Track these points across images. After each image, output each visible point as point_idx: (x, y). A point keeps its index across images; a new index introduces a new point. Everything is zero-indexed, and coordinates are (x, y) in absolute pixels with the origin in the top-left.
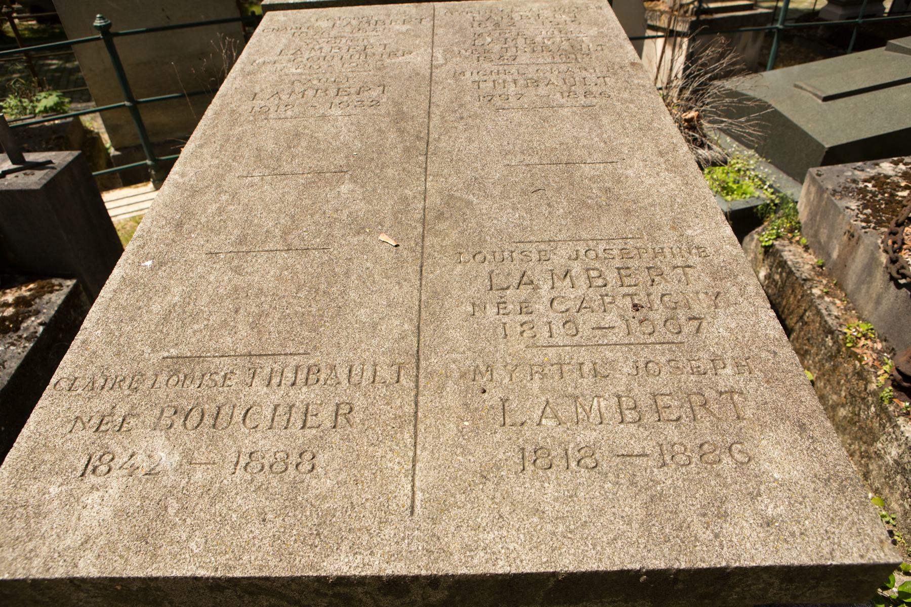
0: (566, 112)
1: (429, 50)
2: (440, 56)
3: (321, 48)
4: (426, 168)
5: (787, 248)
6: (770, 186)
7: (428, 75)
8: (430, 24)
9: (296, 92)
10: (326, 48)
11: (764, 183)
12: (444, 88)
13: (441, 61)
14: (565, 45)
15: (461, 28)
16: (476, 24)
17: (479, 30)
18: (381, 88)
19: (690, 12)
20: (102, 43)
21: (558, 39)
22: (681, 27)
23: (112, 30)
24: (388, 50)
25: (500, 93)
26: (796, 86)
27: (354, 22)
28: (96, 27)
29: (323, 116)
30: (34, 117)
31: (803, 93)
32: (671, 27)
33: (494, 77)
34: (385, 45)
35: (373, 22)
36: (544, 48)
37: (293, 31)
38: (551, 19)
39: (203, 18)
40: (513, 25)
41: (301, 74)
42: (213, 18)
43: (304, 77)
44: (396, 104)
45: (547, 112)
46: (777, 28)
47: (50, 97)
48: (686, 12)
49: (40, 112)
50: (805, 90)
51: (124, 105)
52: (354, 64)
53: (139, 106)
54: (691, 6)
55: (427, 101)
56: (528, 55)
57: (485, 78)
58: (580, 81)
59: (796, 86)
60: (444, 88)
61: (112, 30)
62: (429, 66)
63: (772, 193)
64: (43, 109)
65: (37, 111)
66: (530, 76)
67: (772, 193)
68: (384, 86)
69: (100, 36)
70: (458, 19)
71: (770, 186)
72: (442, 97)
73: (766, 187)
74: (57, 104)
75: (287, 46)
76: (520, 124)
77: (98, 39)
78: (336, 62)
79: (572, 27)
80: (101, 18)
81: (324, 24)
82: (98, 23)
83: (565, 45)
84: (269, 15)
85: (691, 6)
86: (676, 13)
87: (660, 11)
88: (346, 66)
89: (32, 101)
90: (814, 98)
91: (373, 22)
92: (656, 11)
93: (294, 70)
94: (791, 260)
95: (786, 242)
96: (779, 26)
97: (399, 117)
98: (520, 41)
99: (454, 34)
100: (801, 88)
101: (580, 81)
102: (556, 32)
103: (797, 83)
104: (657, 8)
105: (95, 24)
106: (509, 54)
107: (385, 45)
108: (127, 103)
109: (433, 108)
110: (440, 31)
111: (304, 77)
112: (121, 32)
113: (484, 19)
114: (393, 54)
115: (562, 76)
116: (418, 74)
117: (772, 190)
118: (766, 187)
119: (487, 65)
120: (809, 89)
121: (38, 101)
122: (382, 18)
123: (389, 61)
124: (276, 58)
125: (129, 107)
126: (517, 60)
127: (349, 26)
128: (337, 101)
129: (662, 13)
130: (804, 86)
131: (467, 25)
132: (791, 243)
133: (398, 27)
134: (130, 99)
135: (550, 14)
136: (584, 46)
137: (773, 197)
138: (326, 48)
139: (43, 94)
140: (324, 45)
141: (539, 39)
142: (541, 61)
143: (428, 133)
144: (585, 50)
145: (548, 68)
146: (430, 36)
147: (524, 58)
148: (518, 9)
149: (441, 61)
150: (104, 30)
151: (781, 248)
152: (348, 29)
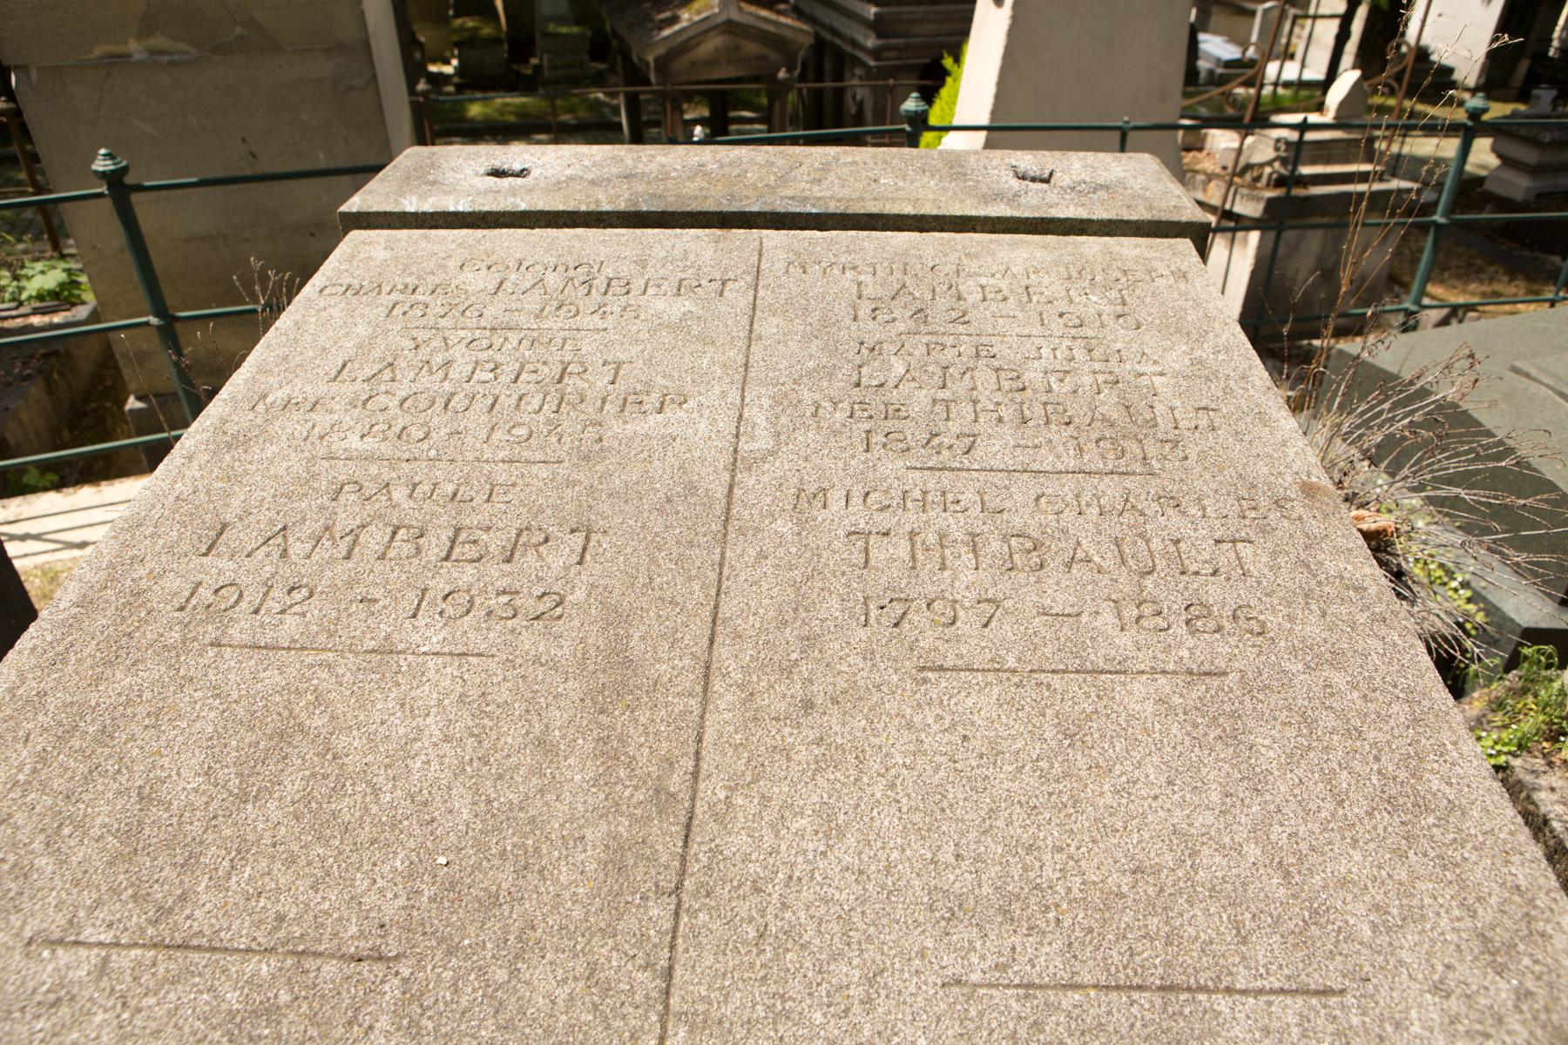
0: (1137, 696)
1: (734, 396)
2: (761, 421)
3: (448, 364)
4: (669, 973)
5: (1543, 781)
6: (1465, 585)
7: (720, 493)
8: (744, 302)
9: (337, 531)
10: (462, 360)
11: (1450, 574)
12: (762, 556)
13: (763, 442)
14: (1109, 403)
15: (825, 323)
16: (865, 310)
17: (873, 331)
18: (579, 539)
19: (1264, 180)
20: (107, 204)
21: (1087, 380)
22: (1250, 208)
23: (129, 180)
24: (622, 385)
25: (931, 590)
26: (1515, 370)
27: (553, 280)
28: (96, 172)
29: (387, 650)
30: (16, 308)
31: (1533, 387)
32: (1227, 207)
33: (912, 519)
34: (619, 365)
35: (600, 283)
36: (1059, 416)
37: (395, 296)
38: (1062, 306)
39: (322, 160)
40: (963, 319)
41: (370, 458)
42: (342, 163)
43: (374, 470)
44: (616, 618)
45: (1077, 695)
46: (1435, 223)
47: (52, 272)
48: (1257, 179)
49: (30, 298)
50: (1535, 380)
51: (147, 324)
52: (522, 432)
53: (178, 327)
54: (1268, 170)
55: (706, 613)
56: (1008, 434)
57: (885, 520)
58: (1165, 554)
59: (1515, 370)
60: (762, 556)
61: (129, 180)
62: (726, 458)
63: (1469, 600)
64: (34, 293)
65: (24, 296)
66: (1017, 522)
67: (1469, 600)
68: (589, 532)
69: (104, 189)
70: (818, 290)
71: (1465, 585)
72: (754, 598)
73: (1454, 584)
74: (62, 285)
75: (364, 348)
76: (995, 753)
77: (100, 195)
78: (476, 420)
79: (1119, 337)
80: (109, 156)
81: (478, 281)
82: (101, 165)
83: (1109, 403)
84: (355, 234)
85: (1268, 170)
86: (1236, 179)
87: (1205, 173)
88: (498, 435)
89: (16, 278)
90: (1558, 399)
91: (600, 283)
92: (1197, 172)
93: (354, 442)
94: (1559, 818)
95: (1539, 762)
96: (1438, 218)
97: (616, 679)
98: (984, 376)
99: (806, 340)
100: (1528, 376)
101: (1165, 554)
102: (1079, 354)
103: (1519, 364)
104: (1198, 167)
105: (94, 167)
106: (955, 427)
107: (619, 365)
108: (153, 320)
109: (723, 651)
110: (768, 326)
111: (374, 470)
112: (147, 184)
113: (886, 293)
114: (631, 403)
115: (1112, 527)
116: (692, 488)
117: (1468, 593)
118: (1454, 584)
119: (891, 467)
120: (1546, 381)
121: (29, 278)
122: (626, 269)
123: (617, 427)
124: (322, 389)
125: (158, 327)
126: (978, 453)
127: (536, 295)
128: (440, 586)
129: (1210, 177)
130: (1533, 372)
131: (842, 311)
132: (1550, 764)
133: (660, 304)
134: (160, 309)
135: (1057, 289)
136: (1160, 409)
137: (1471, 607)
138: (462, 360)
139: (39, 266)
140: (458, 352)
141: (1032, 375)
142: (1047, 461)
143: (695, 774)
144: (1164, 424)
145: (1068, 486)
146: (742, 344)
147: (998, 447)
148: (973, 266)
149: (763, 442)
150: (114, 180)
151: (1529, 778)
152: (533, 301)
